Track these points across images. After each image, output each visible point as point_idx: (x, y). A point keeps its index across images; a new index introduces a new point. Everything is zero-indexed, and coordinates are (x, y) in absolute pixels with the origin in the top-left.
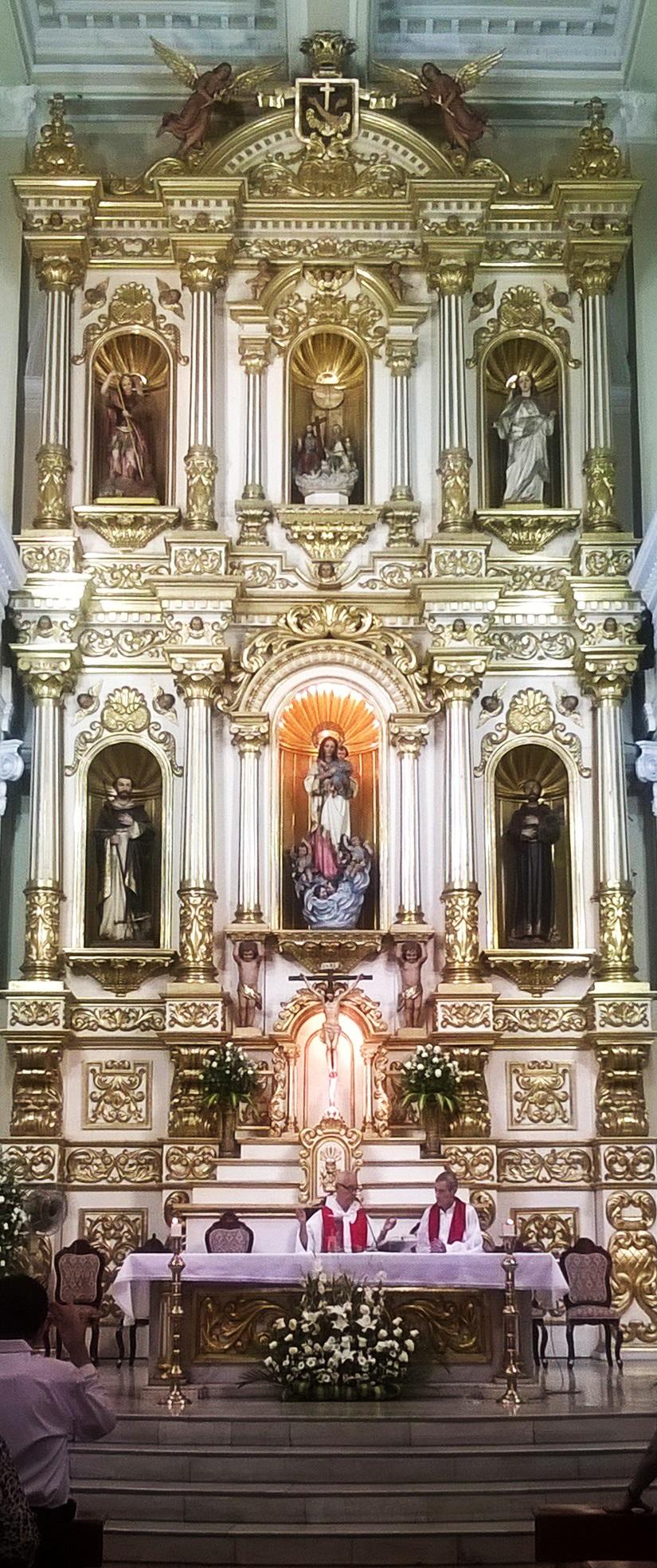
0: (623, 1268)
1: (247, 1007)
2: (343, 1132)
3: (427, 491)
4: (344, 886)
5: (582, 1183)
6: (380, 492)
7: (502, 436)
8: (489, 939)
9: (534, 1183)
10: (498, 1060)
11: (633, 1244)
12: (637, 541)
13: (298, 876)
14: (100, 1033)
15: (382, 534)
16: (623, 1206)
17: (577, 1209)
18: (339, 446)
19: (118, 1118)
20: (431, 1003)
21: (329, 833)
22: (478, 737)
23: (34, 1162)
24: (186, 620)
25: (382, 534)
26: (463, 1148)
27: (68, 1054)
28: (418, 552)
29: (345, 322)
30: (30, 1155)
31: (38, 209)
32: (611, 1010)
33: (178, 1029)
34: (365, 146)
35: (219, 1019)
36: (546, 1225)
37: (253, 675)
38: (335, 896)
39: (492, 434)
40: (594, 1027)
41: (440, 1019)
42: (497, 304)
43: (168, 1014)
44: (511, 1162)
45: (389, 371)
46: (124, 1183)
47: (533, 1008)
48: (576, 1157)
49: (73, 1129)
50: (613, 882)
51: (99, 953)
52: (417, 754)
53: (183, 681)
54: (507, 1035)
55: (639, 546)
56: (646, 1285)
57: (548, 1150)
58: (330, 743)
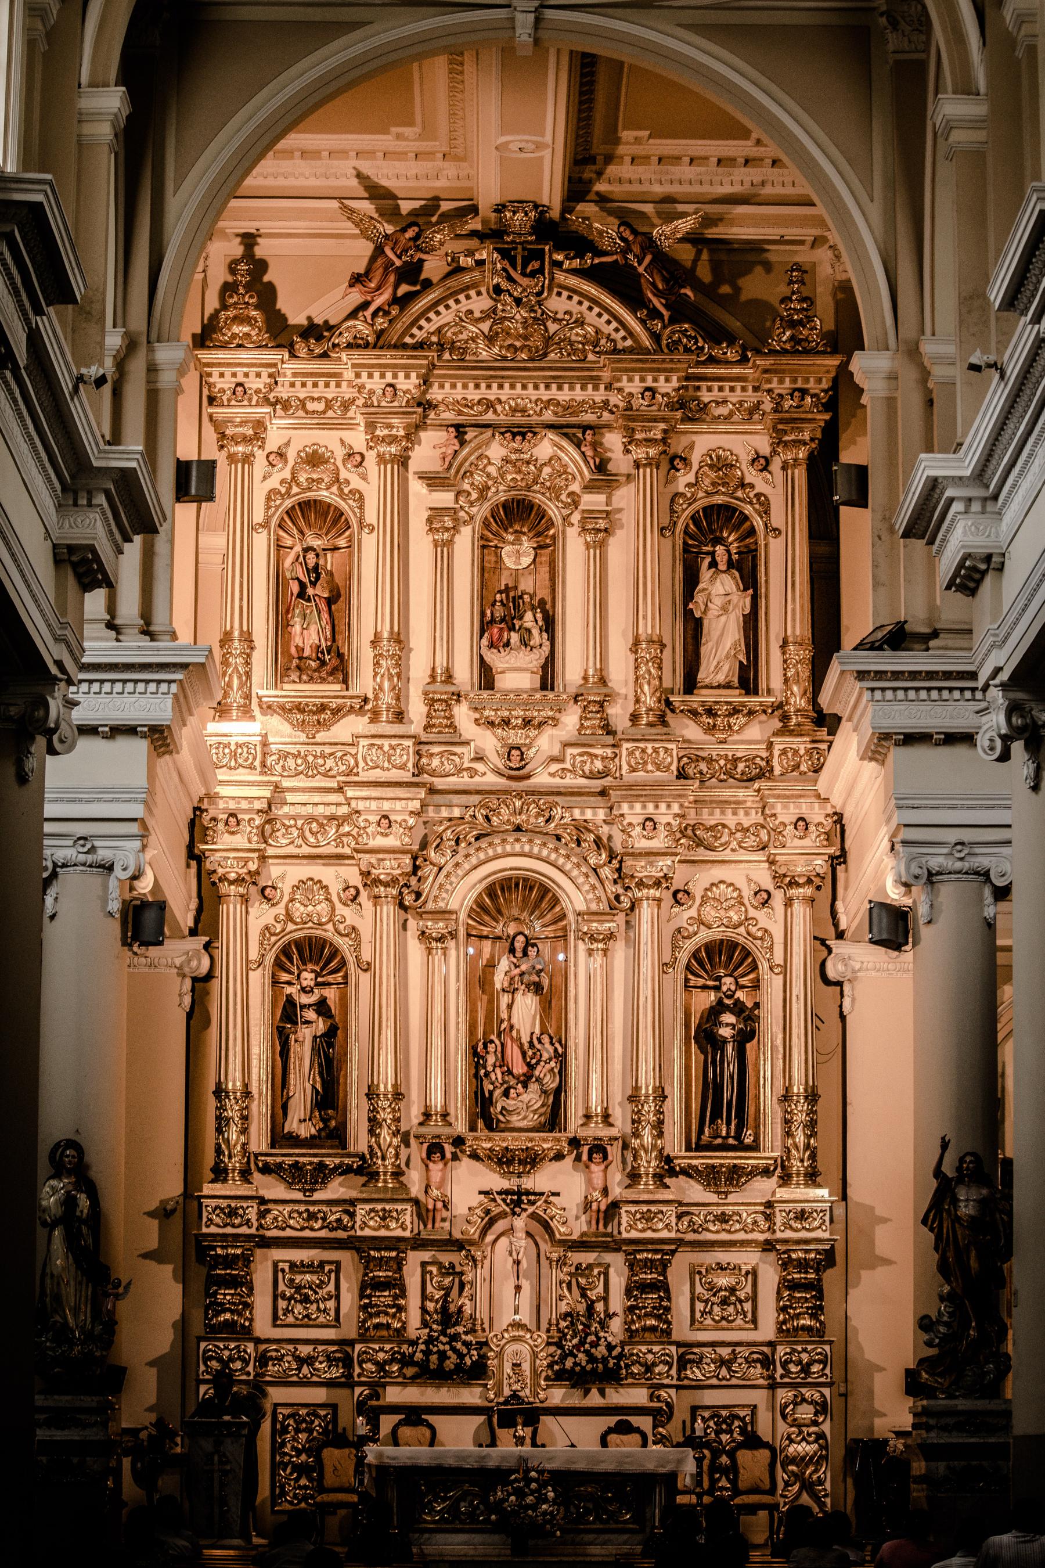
0: (793, 1461)
1: (435, 1209)
2: (528, 1336)
3: (620, 671)
4: (533, 1087)
5: (761, 1382)
6: (573, 669)
7: (698, 615)
8: (674, 1143)
9: (714, 1382)
10: (680, 1265)
11: (804, 1439)
12: (830, 738)
13: (487, 1074)
14: (289, 1233)
15: (571, 719)
16: (796, 1404)
17: (755, 1406)
18: (529, 616)
19: (307, 1316)
20: (615, 1205)
21: (518, 1031)
22: (668, 931)
23: (231, 1359)
24: (374, 818)
25: (571, 719)
26: (644, 1349)
27: (259, 1252)
28: (609, 739)
29: (537, 487)
30: (226, 1353)
31: (223, 383)
32: (792, 1215)
33: (213, 1230)
34: (557, 304)
35: (408, 1223)
36: (724, 1422)
37: (440, 869)
38: (525, 1097)
39: (688, 614)
40: (774, 1231)
41: (624, 1224)
42: (695, 467)
43: (358, 1218)
44: (693, 1361)
45: (581, 540)
46: (315, 1379)
47: (719, 1210)
48: (755, 1356)
49: (263, 1327)
50: (798, 1088)
51: (287, 1157)
52: (605, 951)
53: (370, 880)
54: (690, 1237)
55: (831, 743)
56: (815, 1477)
57: (729, 1350)
58: (521, 938)
